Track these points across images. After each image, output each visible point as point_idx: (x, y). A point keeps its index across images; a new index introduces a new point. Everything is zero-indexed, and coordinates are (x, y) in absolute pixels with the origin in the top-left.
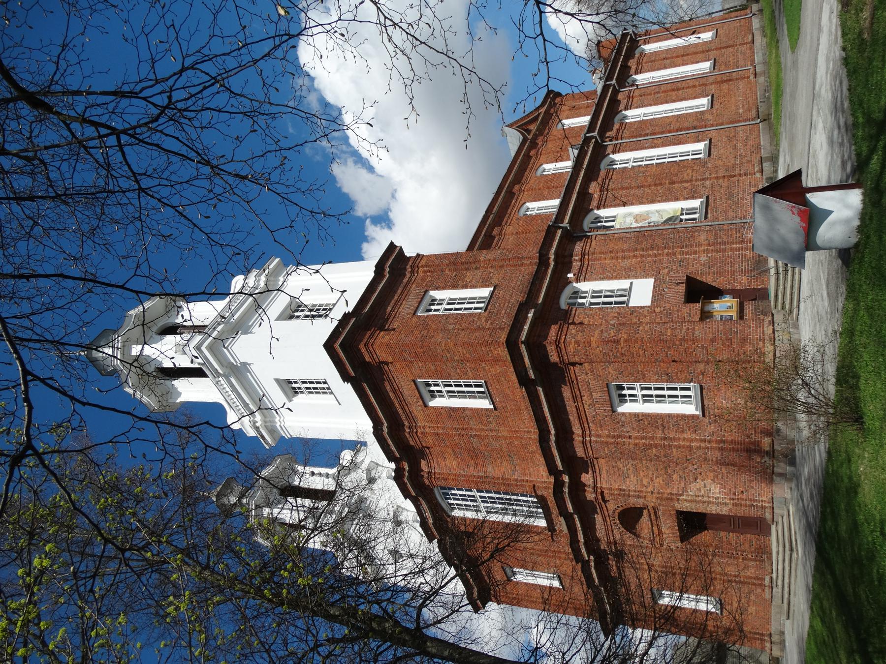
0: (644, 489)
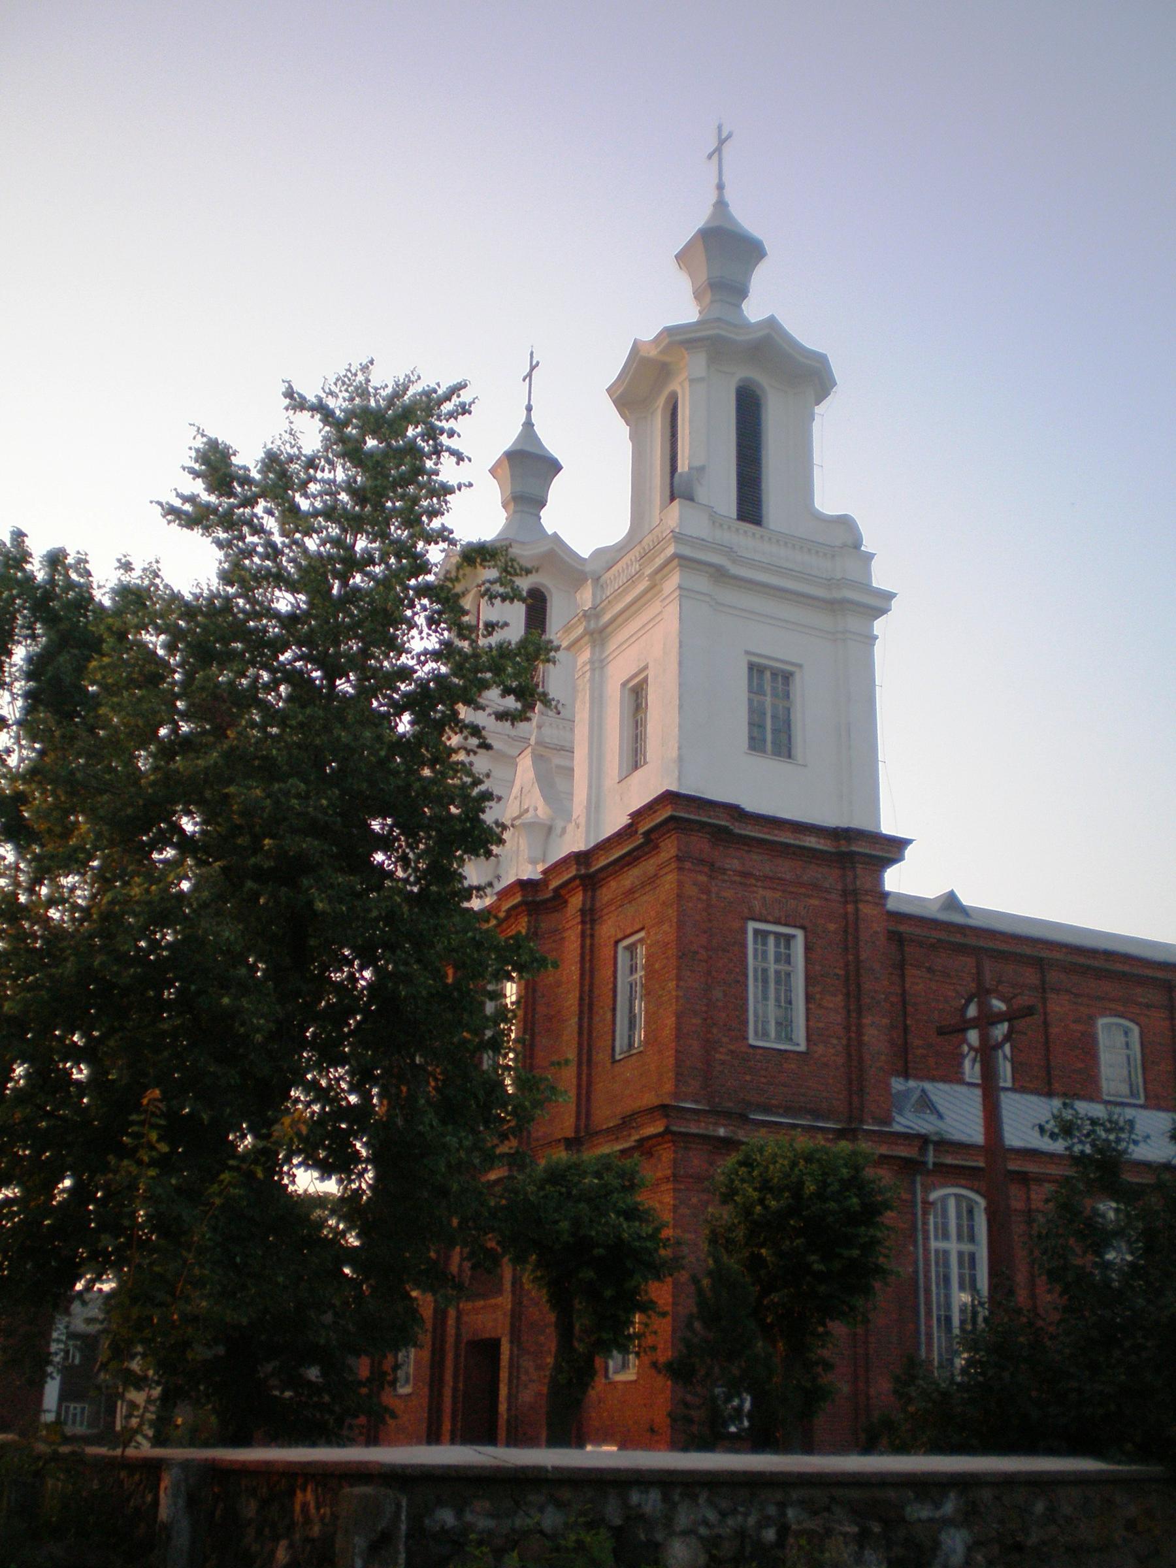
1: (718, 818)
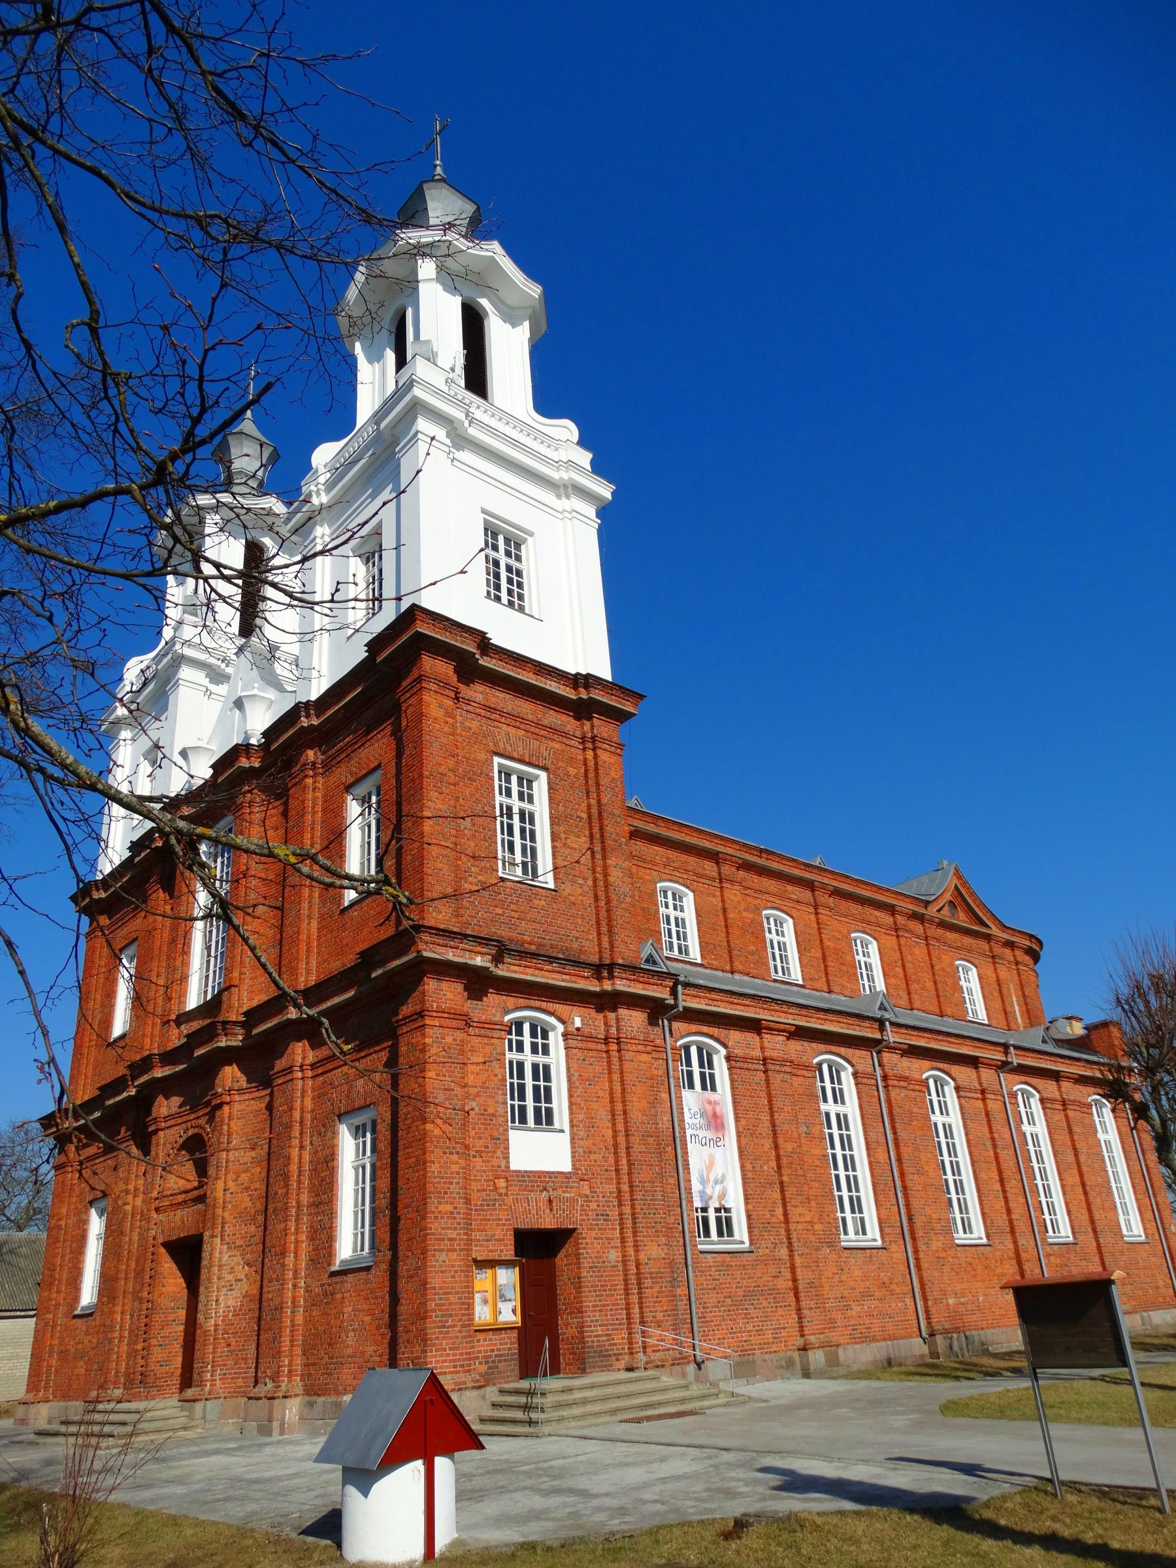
0: (231, 1176)
1: (468, 645)
